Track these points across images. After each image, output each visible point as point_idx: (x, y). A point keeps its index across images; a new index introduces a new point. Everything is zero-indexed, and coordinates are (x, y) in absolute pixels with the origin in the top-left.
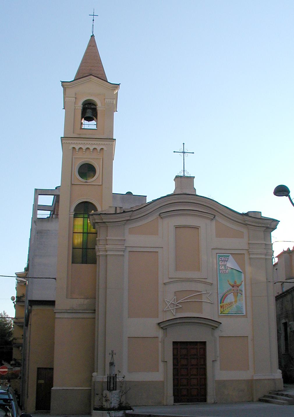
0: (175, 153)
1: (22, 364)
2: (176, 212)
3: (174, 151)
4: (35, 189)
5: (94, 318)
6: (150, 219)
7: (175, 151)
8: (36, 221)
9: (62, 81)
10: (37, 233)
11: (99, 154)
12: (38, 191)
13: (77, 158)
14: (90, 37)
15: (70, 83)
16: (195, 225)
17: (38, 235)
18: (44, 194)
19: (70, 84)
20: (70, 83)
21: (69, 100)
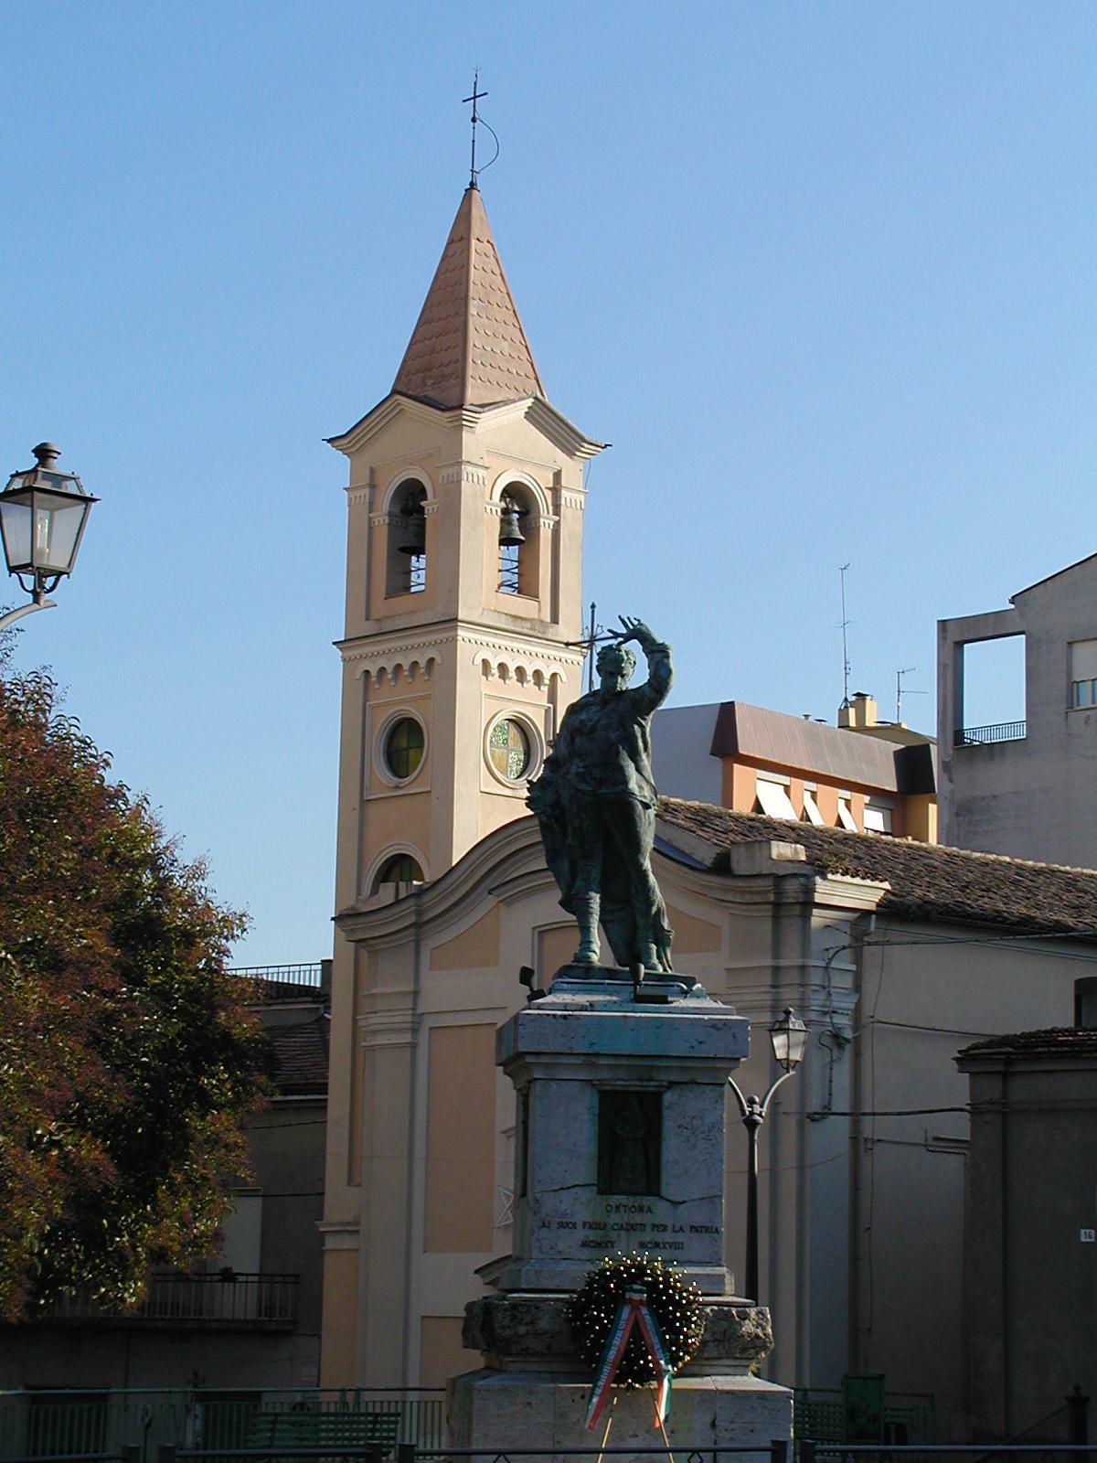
0: (590, 610)
1: (295, 1412)
2: (544, 878)
3: (596, 604)
4: (938, 621)
5: (707, 1229)
6: (479, 913)
7: (596, 610)
8: (949, 762)
9: (327, 438)
10: (957, 815)
11: (410, 683)
12: (950, 627)
13: (378, 706)
14: (464, 192)
15: (349, 439)
16: (545, 923)
17: (959, 825)
18: (983, 635)
19: (351, 441)
20: (349, 439)
21: (356, 497)
